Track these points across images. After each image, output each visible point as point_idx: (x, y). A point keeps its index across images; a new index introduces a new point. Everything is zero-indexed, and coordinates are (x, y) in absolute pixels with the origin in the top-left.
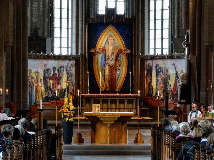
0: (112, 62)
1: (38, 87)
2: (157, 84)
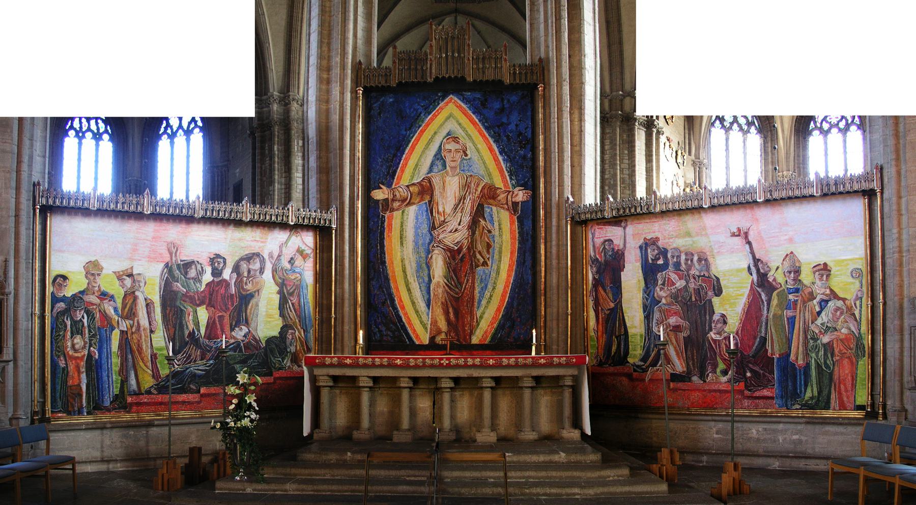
0: (457, 234)
1: (135, 336)
2: (648, 317)
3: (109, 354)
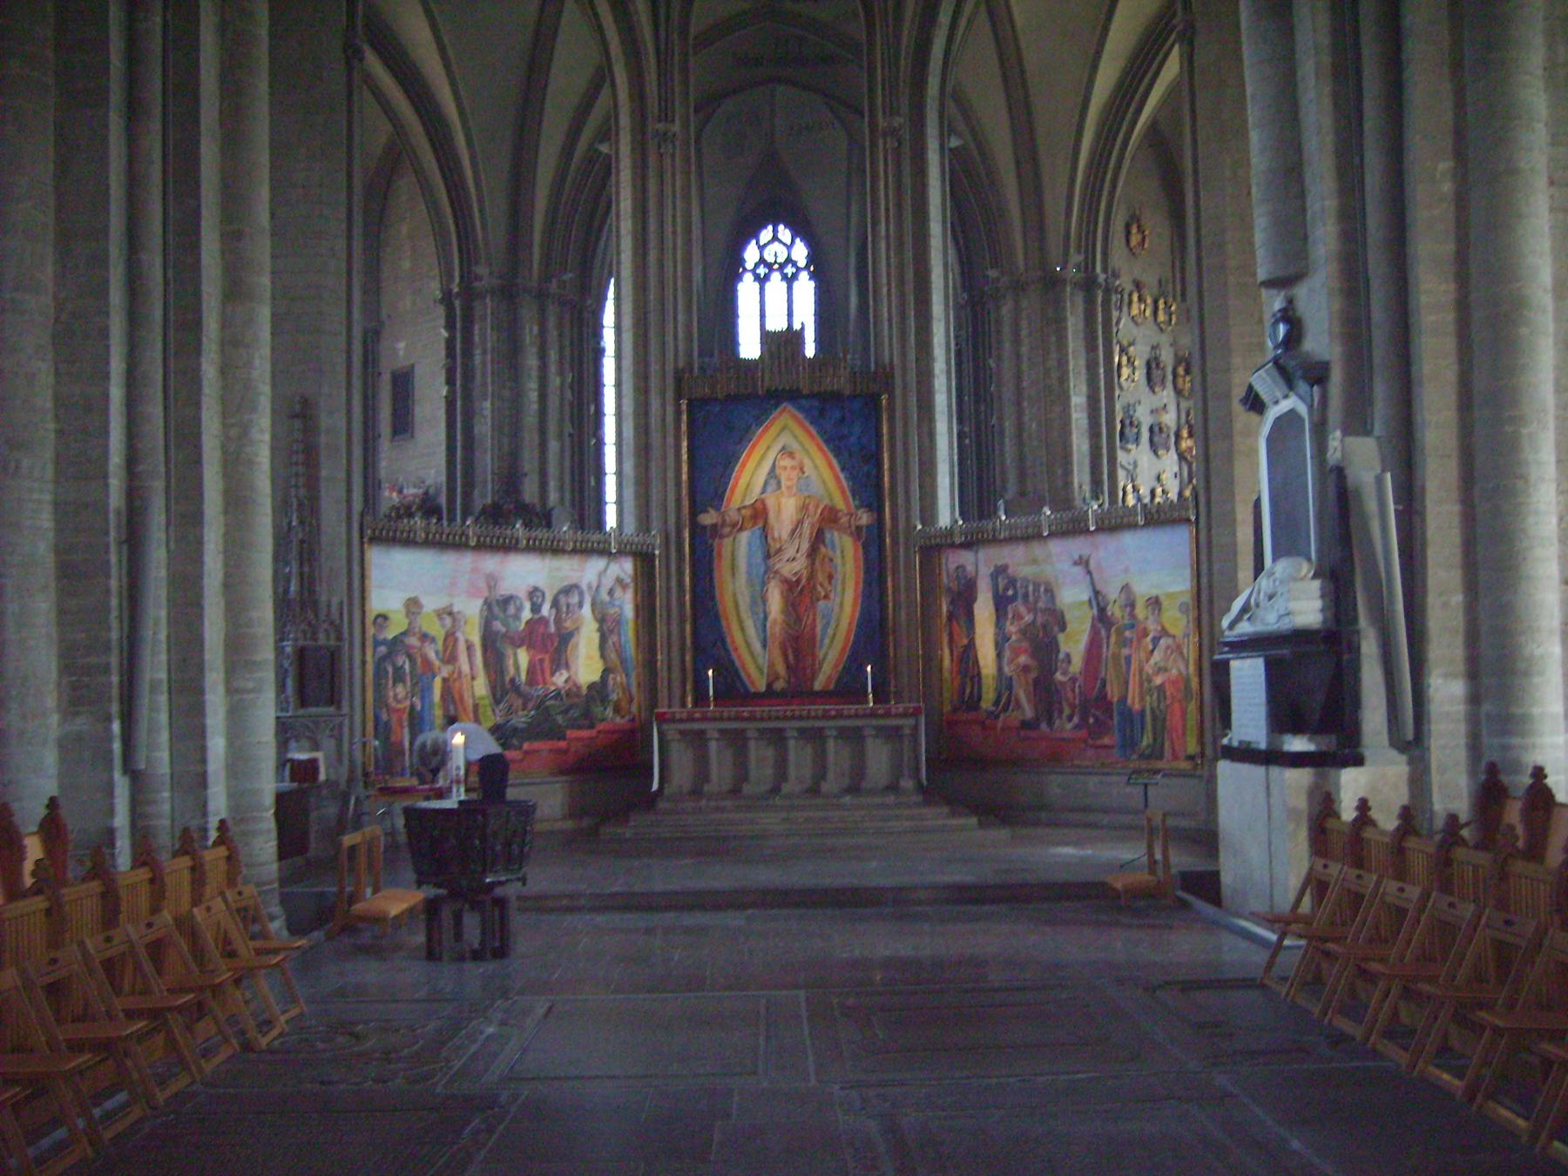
0: (794, 564)
2: (999, 656)
3: (431, 703)
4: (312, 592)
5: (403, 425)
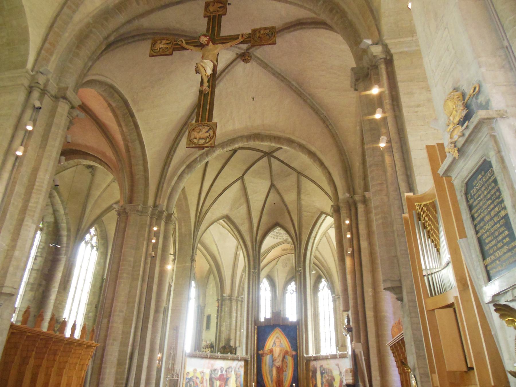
4: (173, 367)
5: (208, 327)
